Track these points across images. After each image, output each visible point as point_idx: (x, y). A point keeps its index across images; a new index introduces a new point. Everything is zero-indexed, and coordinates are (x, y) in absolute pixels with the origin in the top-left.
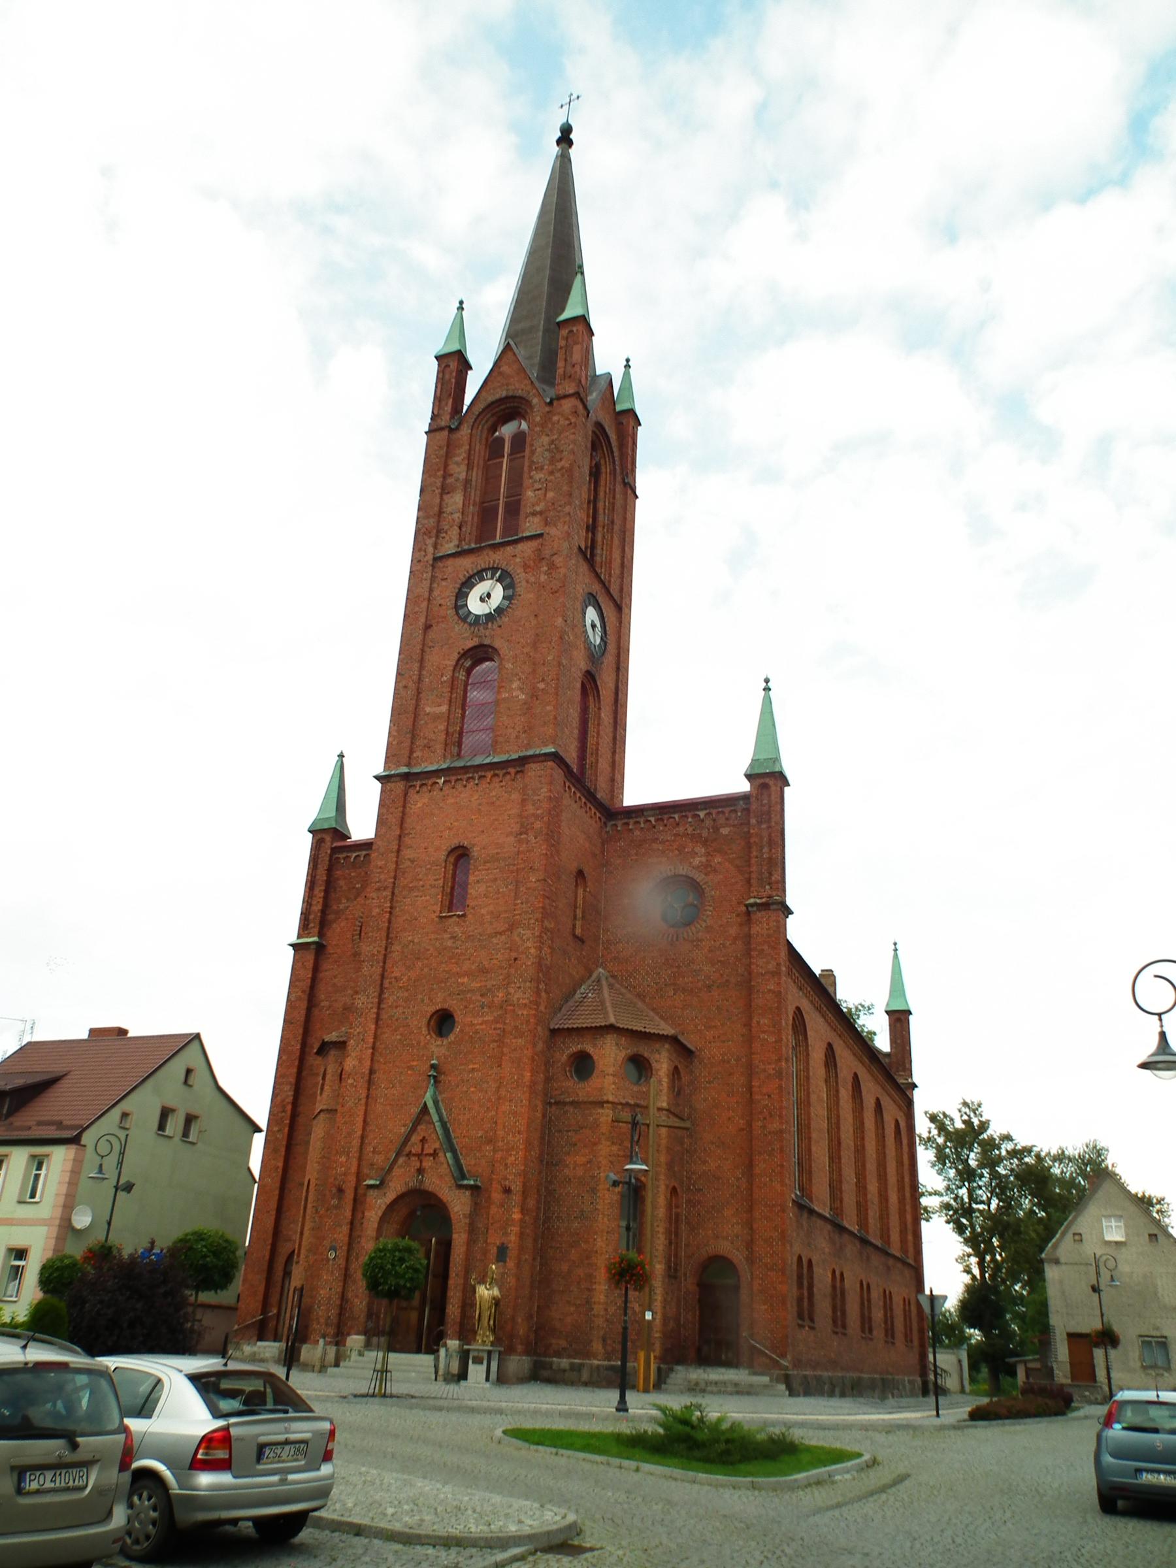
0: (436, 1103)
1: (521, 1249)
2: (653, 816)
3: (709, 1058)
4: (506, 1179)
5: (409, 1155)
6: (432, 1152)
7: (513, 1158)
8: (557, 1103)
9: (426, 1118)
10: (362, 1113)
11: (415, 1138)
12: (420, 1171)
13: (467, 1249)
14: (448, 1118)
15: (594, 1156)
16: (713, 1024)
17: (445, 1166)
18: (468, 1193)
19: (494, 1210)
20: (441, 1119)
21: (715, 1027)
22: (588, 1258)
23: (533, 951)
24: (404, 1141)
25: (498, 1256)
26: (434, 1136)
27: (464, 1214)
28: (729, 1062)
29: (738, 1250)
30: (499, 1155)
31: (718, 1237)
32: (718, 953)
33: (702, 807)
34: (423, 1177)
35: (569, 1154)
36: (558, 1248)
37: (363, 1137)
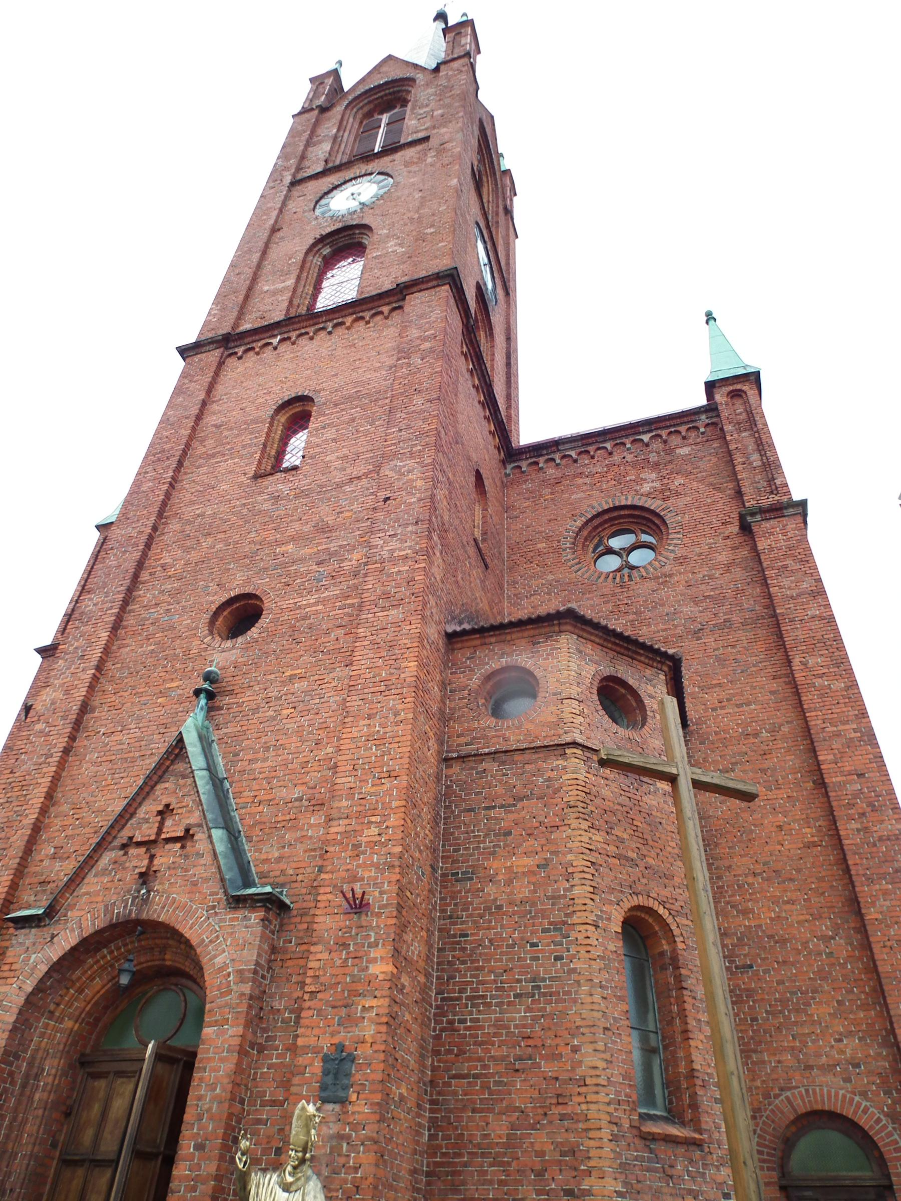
0: (205, 743)
1: (391, 1059)
2: (572, 449)
3: (717, 733)
4: (355, 879)
5: (130, 843)
6: (180, 834)
7: (374, 830)
8: (462, 758)
9: (180, 767)
10: (46, 781)
11: (149, 809)
12: (145, 877)
13: (239, 1070)
14: (227, 771)
15: (555, 853)
16: (714, 682)
17: (207, 859)
18: (255, 917)
19: (319, 956)
20: (210, 768)
21: (719, 685)
22: (561, 1099)
23: (419, 483)
24: (121, 815)
25: (324, 1088)
26: (189, 801)
27: (240, 972)
28: (756, 735)
29: (864, 1094)
30: (337, 828)
31: (809, 1068)
32: (703, 587)
33: (646, 428)
34: (148, 892)
35: (494, 853)
36: (476, 1076)
37: (37, 829)
